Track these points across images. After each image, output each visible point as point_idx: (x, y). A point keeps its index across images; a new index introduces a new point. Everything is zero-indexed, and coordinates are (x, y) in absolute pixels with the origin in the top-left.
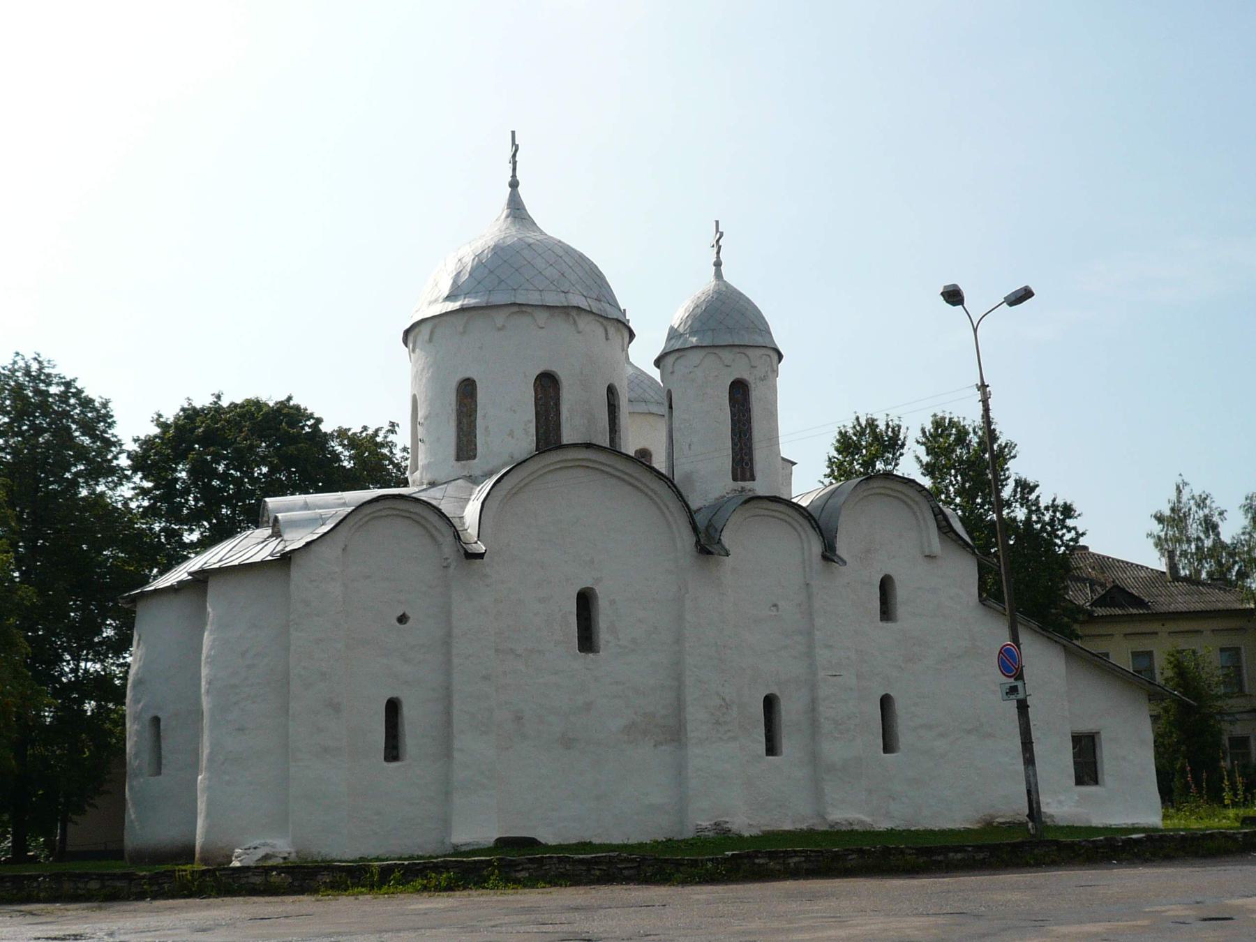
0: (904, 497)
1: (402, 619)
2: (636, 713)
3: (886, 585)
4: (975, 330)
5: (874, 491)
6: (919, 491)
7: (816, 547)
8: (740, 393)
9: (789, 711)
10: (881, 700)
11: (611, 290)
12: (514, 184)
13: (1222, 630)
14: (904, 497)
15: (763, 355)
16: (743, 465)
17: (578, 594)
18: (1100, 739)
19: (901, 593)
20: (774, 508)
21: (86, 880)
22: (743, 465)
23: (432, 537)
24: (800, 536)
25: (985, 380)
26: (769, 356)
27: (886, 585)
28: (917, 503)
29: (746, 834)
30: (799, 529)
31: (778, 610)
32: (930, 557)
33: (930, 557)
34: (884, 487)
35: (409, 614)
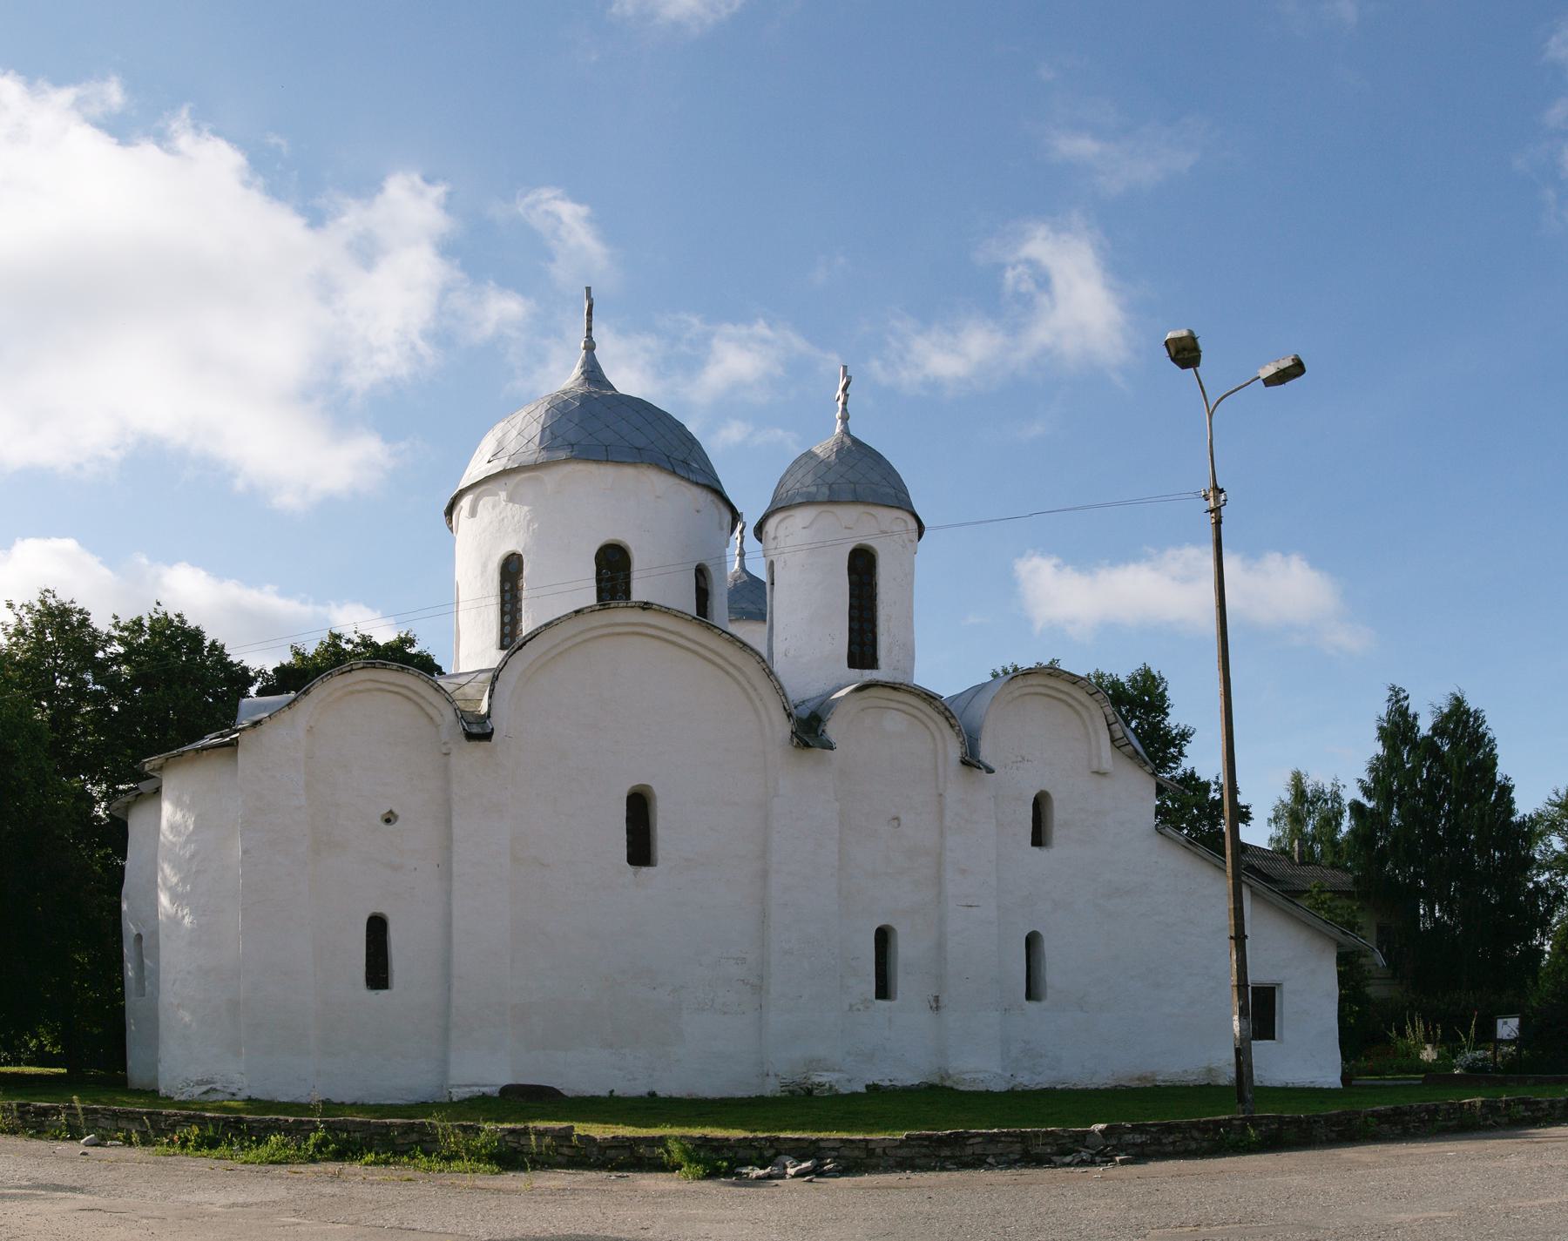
0: (1070, 701)
2: (356, 632)
3: (1040, 805)
4: (1211, 416)
5: (1032, 690)
6: (1091, 695)
7: (955, 751)
8: (862, 565)
9: (904, 950)
10: (1027, 938)
11: (704, 452)
12: (590, 347)
13: (1331, 938)
14: (1070, 701)
15: (898, 518)
16: (863, 650)
17: (629, 798)
18: (1281, 993)
19: (1059, 814)
20: (900, 699)
21: (1029, 1159)
22: (863, 650)
24: (932, 734)
25: (1218, 484)
26: (905, 522)
27: (1040, 805)
28: (1087, 708)
29: (843, 1091)
30: (931, 725)
31: (899, 825)
32: (1099, 773)
33: (1099, 773)
34: (1046, 686)
35: (396, 811)
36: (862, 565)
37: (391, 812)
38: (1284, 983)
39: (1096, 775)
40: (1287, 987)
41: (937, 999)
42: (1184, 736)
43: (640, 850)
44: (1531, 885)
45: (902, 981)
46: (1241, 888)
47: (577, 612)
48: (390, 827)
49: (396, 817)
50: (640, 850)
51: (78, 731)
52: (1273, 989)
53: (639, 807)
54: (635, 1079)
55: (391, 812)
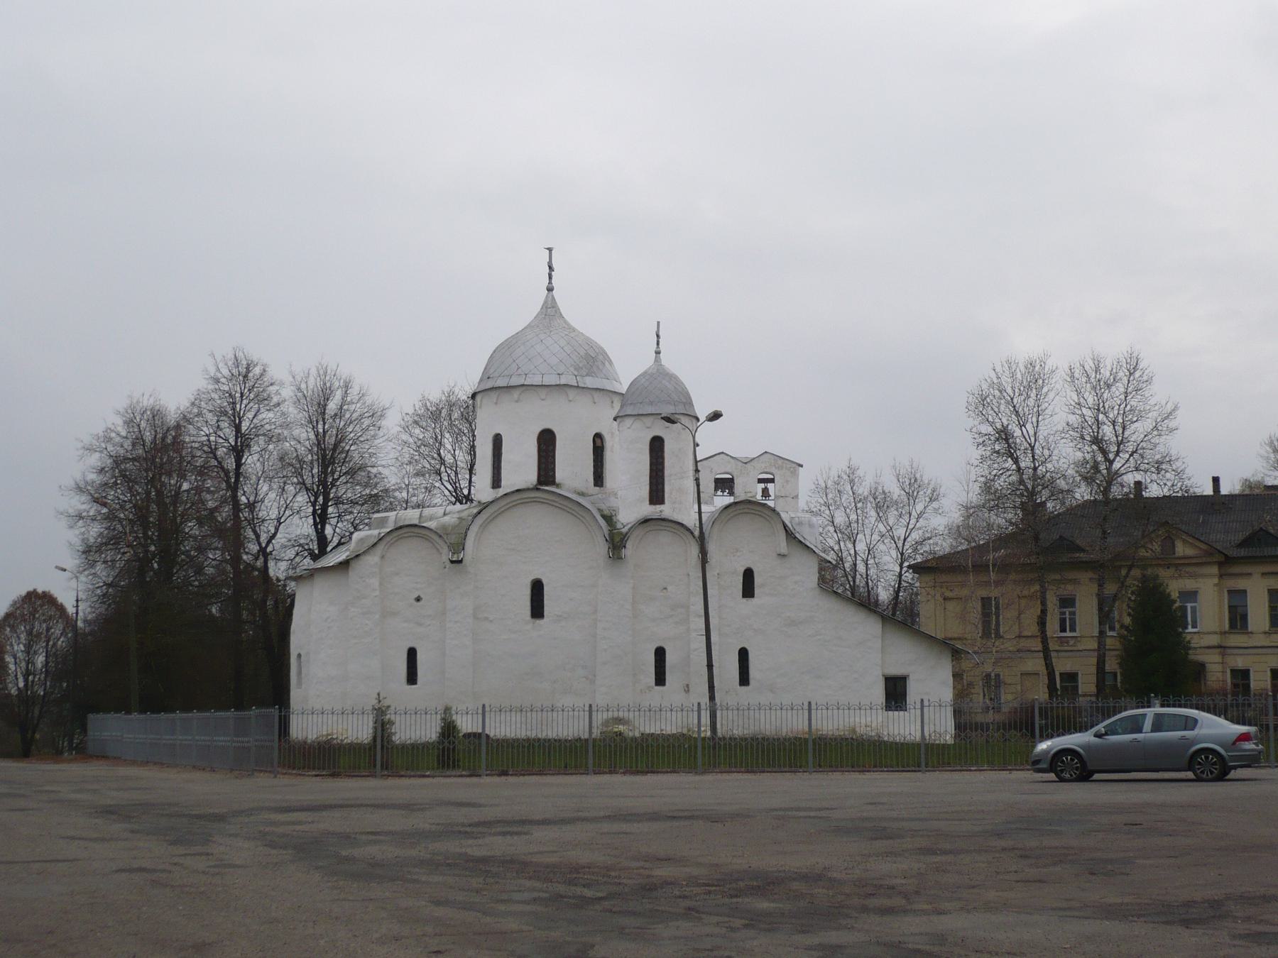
1: (418, 599)
11: (506, 341)
23: (438, 549)
35: (422, 596)
36: (657, 446)
37: (419, 596)
38: (911, 675)
39: (780, 557)
40: (911, 677)
41: (688, 686)
42: (80, 489)
43: (537, 610)
44: (1181, 630)
45: (669, 677)
46: (1195, 775)
47: (505, 494)
48: (418, 604)
49: (422, 599)
50: (537, 610)
51: (231, 576)
52: (906, 678)
53: (537, 588)
54: (410, 843)
55: (419, 596)
